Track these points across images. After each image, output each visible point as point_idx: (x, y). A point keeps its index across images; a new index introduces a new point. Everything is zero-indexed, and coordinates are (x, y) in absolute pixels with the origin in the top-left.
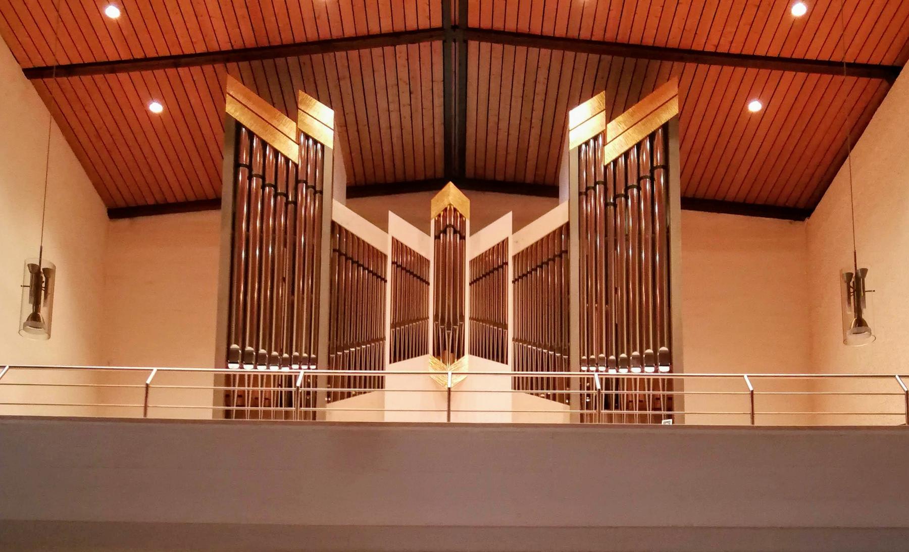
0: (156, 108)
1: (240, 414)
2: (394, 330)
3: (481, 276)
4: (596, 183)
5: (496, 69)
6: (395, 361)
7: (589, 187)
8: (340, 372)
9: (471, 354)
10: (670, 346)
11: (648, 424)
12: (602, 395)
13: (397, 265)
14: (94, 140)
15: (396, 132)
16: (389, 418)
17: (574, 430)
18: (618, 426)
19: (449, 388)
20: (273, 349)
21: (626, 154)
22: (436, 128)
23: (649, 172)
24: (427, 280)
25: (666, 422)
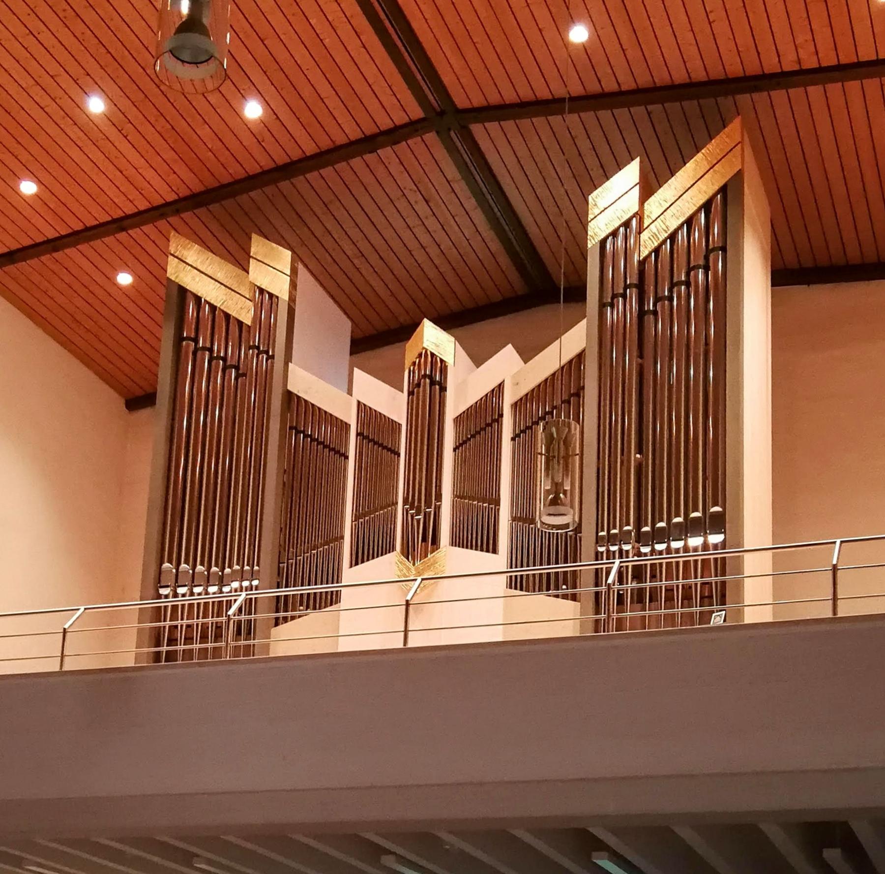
0: (125, 279)
1: (171, 656)
2: (357, 522)
3: (469, 436)
4: (626, 287)
5: (522, 152)
6: (357, 564)
7: (616, 294)
8: (291, 591)
9: (452, 545)
10: (724, 507)
11: (194, 661)
12: (614, 591)
13: (363, 436)
14: (73, 326)
15: (433, 251)
16: (345, 645)
17: (590, 643)
18: (667, 632)
19: (407, 601)
20: (227, 565)
21: (673, 237)
22: (484, 234)
23: (703, 258)
24: (397, 450)
25: (717, 619)
